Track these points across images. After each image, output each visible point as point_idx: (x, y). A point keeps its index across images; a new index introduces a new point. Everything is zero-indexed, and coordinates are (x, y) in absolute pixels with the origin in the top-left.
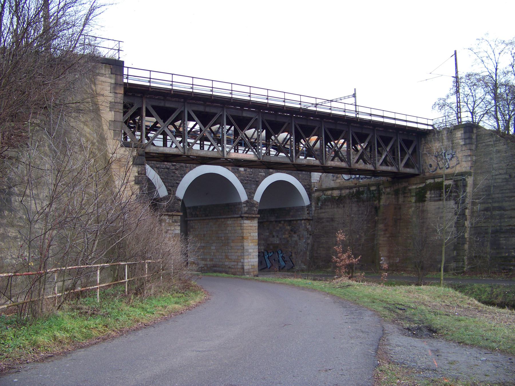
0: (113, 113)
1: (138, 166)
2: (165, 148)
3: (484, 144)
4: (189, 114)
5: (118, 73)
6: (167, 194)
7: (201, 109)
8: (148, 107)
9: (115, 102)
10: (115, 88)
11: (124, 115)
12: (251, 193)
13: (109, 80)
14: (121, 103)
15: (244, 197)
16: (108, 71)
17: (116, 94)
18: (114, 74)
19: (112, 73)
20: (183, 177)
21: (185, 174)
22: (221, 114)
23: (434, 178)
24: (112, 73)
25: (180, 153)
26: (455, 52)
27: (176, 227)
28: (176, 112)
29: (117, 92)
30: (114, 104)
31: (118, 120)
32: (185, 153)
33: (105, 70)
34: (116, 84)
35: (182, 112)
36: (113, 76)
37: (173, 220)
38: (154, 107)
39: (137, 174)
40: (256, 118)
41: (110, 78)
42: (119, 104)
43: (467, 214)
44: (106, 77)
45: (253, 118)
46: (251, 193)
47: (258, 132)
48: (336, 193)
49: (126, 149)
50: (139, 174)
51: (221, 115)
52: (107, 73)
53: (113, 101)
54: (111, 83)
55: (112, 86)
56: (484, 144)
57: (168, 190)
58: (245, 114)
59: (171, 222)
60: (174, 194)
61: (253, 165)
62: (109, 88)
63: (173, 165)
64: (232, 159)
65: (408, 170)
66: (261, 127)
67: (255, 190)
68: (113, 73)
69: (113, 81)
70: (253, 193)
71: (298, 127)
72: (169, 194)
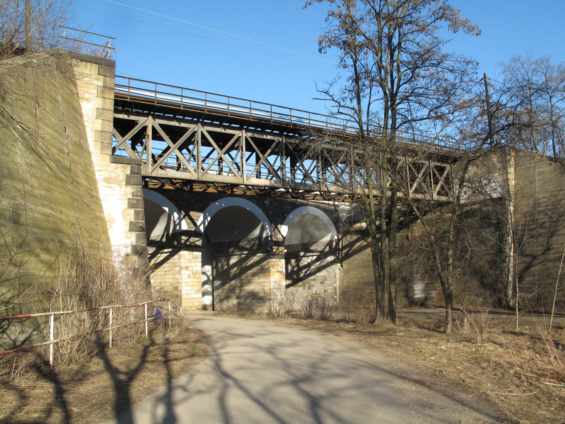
0: (100, 121)
1: (132, 187)
3: (523, 167)
5: (108, 75)
9: (103, 109)
10: (103, 92)
13: (96, 82)
14: (111, 111)
16: (95, 71)
19: (99, 74)
24: (99, 74)
26: (485, 74)
27: (197, 263)
29: (106, 96)
30: (101, 110)
33: (91, 70)
34: (104, 87)
36: (101, 77)
37: (193, 256)
39: (131, 197)
41: (98, 79)
42: (109, 112)
44: (91, 78)
47: (281, 160)
49: (117, 166)
50: (133, 196)
52: (93, 73)
53: (101, 107)
56: (523, 167)
59: (191, 258)
65: (443, 198)
66: (284, 153)
68: (101, 73)
69: (101, 83)
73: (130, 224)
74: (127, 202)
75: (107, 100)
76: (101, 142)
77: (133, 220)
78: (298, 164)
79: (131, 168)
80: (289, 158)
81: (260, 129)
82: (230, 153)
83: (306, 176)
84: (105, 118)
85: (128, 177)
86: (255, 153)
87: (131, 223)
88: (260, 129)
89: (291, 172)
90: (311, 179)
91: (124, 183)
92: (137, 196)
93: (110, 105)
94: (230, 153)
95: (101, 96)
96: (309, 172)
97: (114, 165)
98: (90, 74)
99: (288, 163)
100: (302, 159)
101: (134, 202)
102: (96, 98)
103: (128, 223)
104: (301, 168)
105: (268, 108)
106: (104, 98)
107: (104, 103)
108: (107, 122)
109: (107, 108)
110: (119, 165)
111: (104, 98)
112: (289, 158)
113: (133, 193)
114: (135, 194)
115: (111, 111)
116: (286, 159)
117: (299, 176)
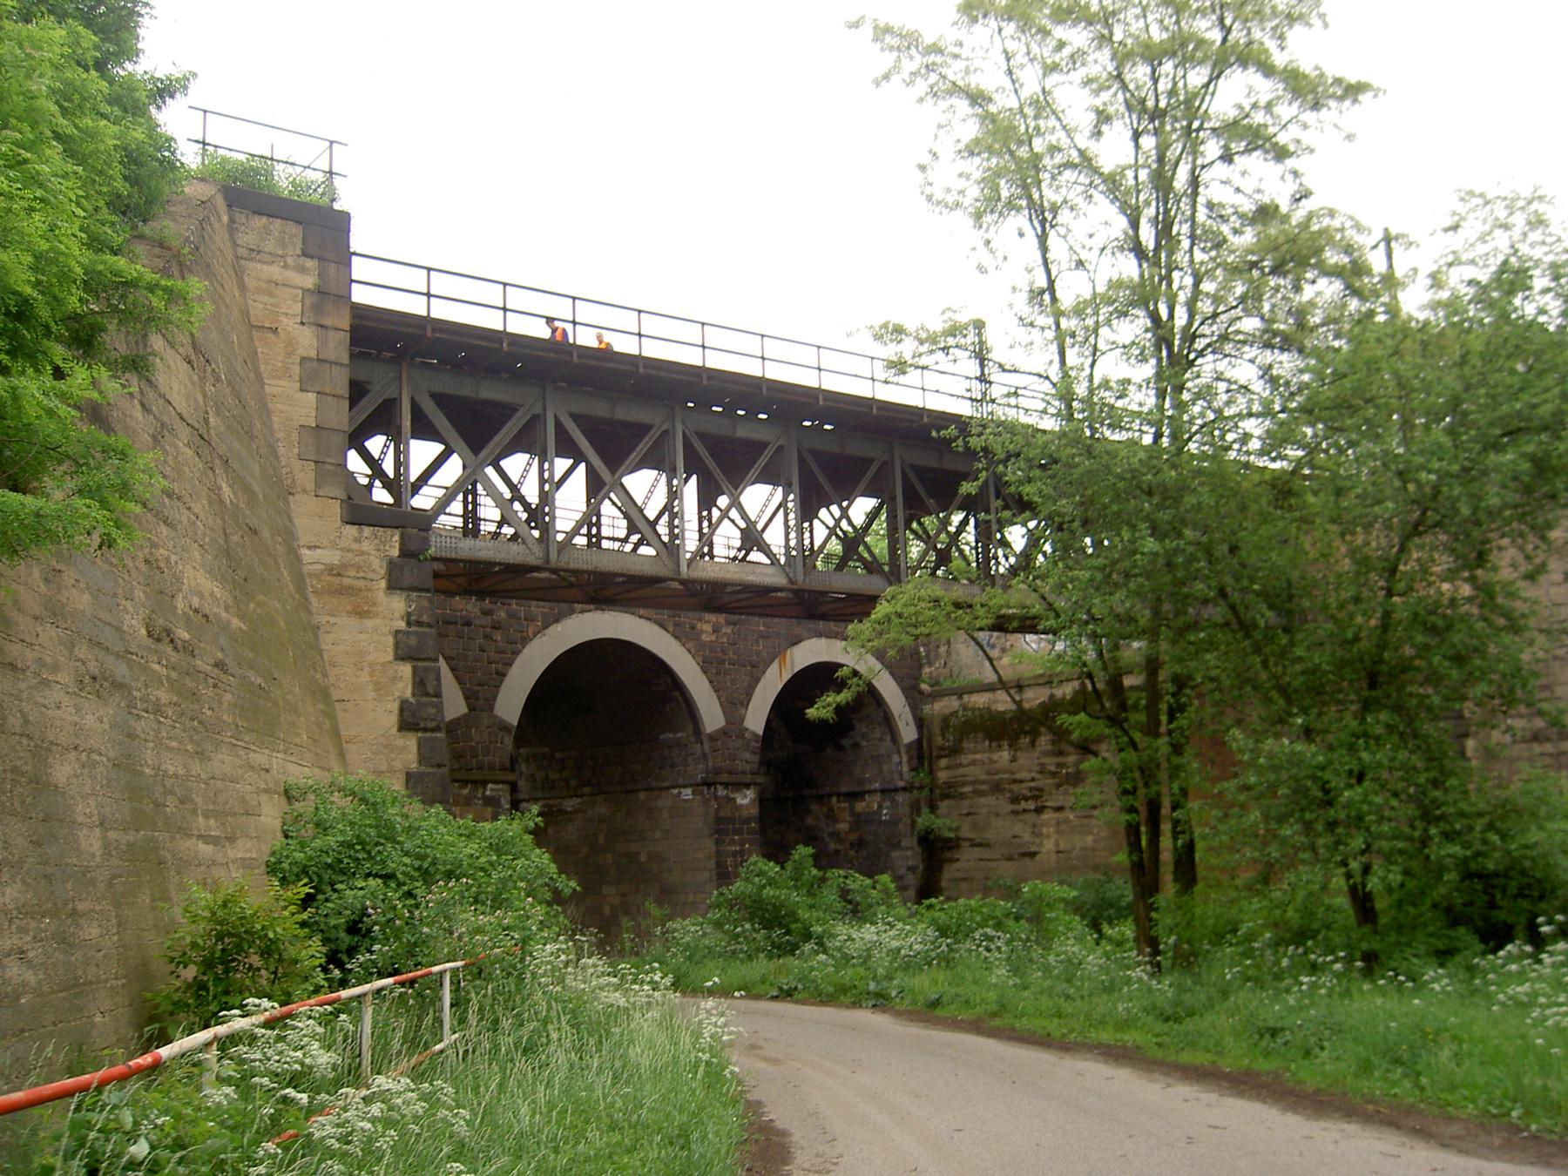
0: (312, 397)
1: (404, 595)
2: (469, 543)
4: (559, 427)
6: (465, 710)
7: (599, 409)
8: (418, 399)
10: (318, 309)
11: (352, 405)
12: (735, 704)
14: (341, 365)
15: (712, 716)
17: (324, 331)
18: (312, 257)
20: (516, 653)
21: (526, 640)
22: (664, 428)
23: (959, 693)
24: (305, 254)
25: (531, 560)
28: (514, 419)
29: (328, 322)
30: (315, 364)
31: (332, 424)
32: (548, 560)
35: (535, 422)
36: (310, 264)
38: (440, 400)
39: (402, 625)
40: (781, 442)
41: (302, 270)
43: (1469, 753)
44: (286, 266)
45: (768, 444)
46: (735, 704)
48: (1002, 702)
50: (409, 624)
51: (666, 432)
53: (313, 354)
54: (306, 291)
55: (308, 301)
57: (467, 698)
58: (743, 432)
60: (492, 708)
61: (749, 607)
62: (297, 308)
63: (486, 613)
64: (701, 582)
67: (749, 695)
70: (742, 704)
71: (912, 475)
72: (472, 709)
73: (401, 710)
74: (390, 640)
75: (332, 334)
76: (316, 462)
77: (408, 693)
78: (723, 501)
79: (402, 537)
80: (694, 478)
81: (764, 416)
82: (503, 463)
83: (752, 538)
84: (327, 389)
85: (392, 566)
86: (583, 465)
87: (404, 706)
88: (720, 409)
89: (599, 516)
90: (765, 549)
91: (383, 584)
92: (419, 623)
93: (338, 346)
94: (503, 463)
95: (312, 320)
96: (760, 527)
97: (352, 530)
98: (280, 253)
99: (691, 490)
100: (736, 483)
101: (413, 641)
102: (301, 327)
103: (396, 706)
104: (734, 513)
105: (752, 344)
106: (322, 326)
107: (323, 343)
108: (330, 398)
109: (332, 358)
110: (367, 531)
111: (322, 326)
112: (694, 478)
113: (409, 614)
114: (413, 618)
115: (341, 365)
116: (686, 480)
117: (727, 539)
